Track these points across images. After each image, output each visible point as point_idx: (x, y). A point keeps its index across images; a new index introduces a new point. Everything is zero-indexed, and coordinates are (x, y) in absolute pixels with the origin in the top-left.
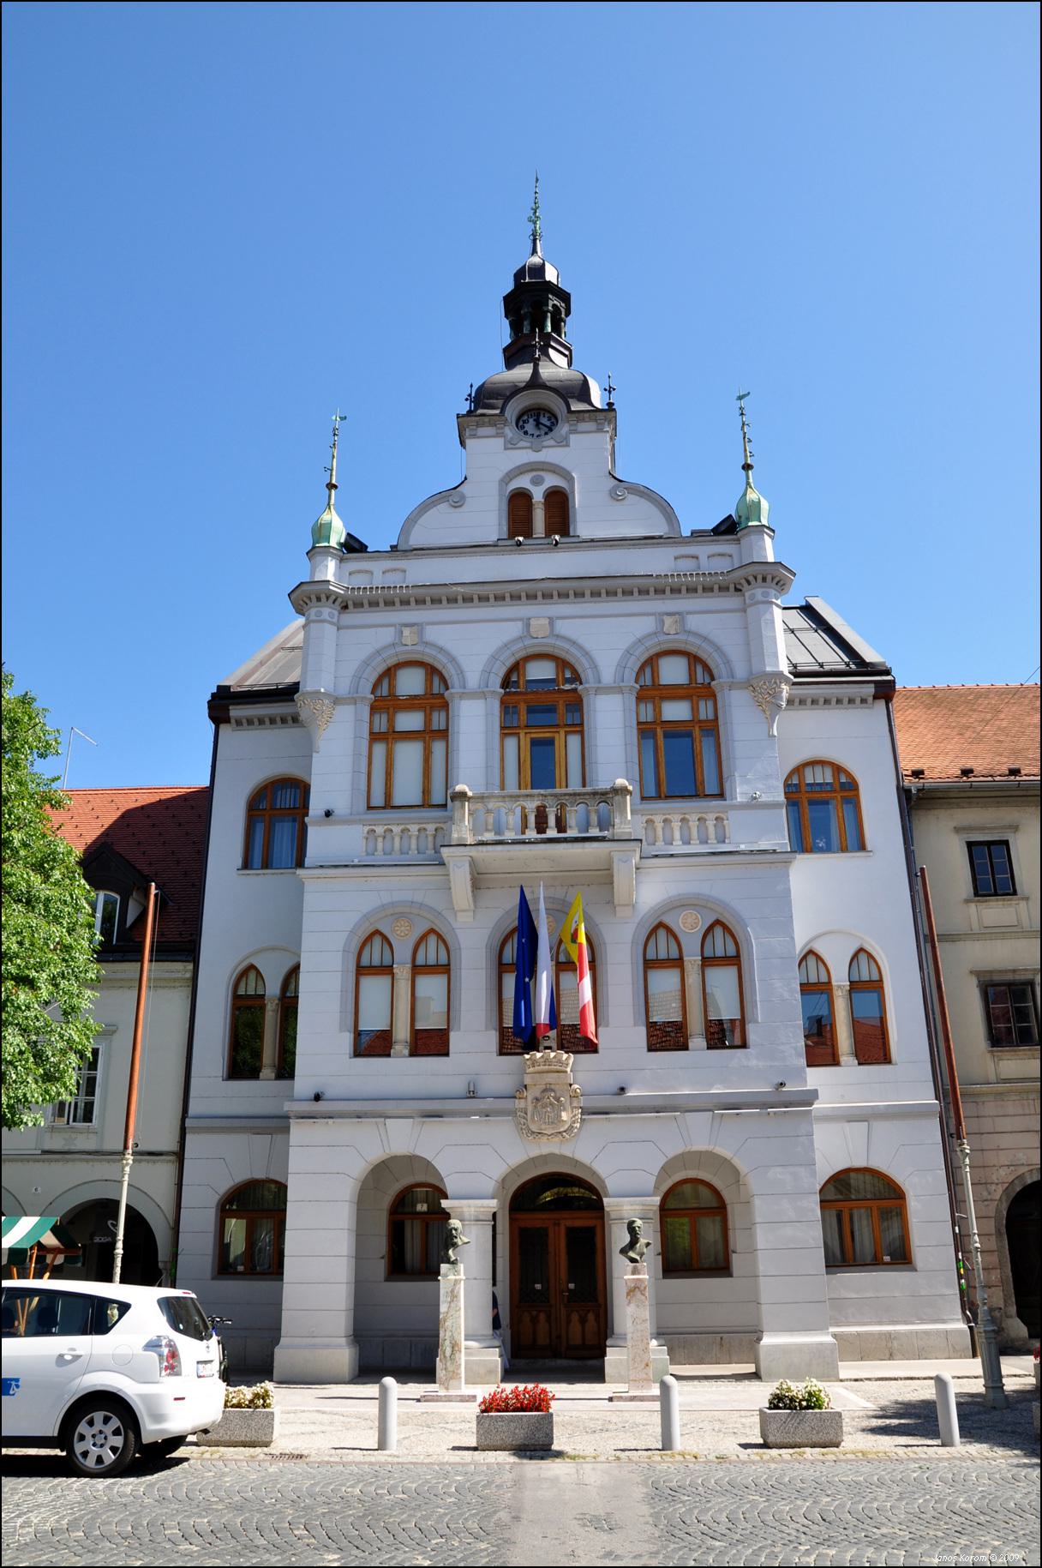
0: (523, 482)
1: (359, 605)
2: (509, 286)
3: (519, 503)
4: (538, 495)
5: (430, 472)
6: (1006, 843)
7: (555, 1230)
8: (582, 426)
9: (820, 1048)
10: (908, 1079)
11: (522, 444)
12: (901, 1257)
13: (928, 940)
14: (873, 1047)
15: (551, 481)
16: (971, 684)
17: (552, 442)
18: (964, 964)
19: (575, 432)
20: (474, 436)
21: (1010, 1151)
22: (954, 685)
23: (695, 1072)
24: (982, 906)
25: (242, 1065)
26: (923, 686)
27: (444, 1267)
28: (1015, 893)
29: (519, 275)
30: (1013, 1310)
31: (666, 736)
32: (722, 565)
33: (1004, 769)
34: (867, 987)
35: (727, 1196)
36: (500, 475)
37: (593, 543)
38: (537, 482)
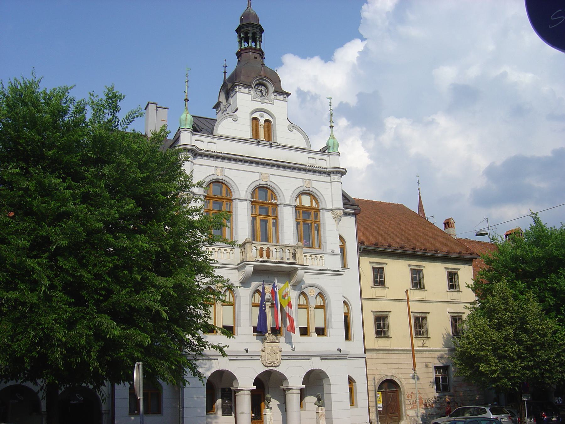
0: (257, 115)
1: (201, 155)
2: (239, 24)
6: (383, 268)
11: (257, 99)
15: (267, 117)
17: (267, 101)
19: (275, 99)
20: (240, 92)
29: (241, 20)
38: (262, 117)
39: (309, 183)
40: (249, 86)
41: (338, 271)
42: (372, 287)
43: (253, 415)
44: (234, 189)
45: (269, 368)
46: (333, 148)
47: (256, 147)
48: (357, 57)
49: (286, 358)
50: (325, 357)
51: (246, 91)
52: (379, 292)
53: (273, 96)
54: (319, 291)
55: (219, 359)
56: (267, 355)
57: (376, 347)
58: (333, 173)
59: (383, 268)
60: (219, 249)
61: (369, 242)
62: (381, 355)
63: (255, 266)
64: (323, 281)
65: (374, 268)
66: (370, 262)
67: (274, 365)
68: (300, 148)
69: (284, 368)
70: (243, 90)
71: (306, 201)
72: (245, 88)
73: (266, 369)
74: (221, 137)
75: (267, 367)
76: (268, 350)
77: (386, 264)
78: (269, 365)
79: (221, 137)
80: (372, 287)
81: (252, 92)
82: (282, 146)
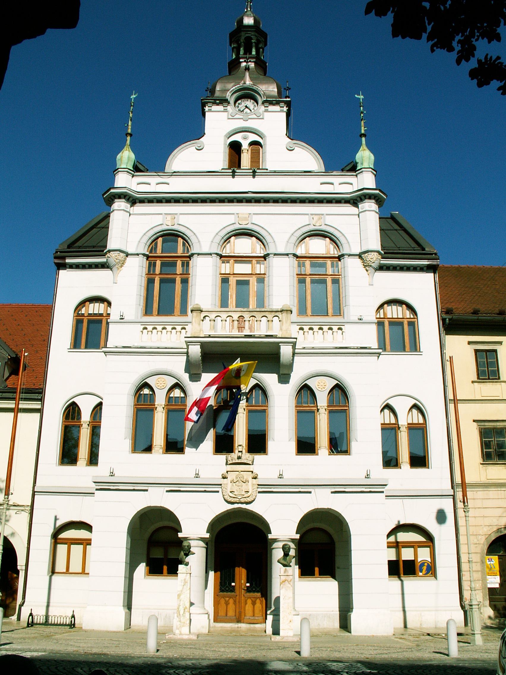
0: (237, 138)
3: (235, 148)
4: (245, 145)
5: (266, 56)
6: (495, 351)
7: (239, 547)
8: (271, 108)
9: (390, 461)
10: (436, 475)
12: (415, 347)
13: (452, 401)
14: (419, 461)
16: (480, 265)
18: (469, 414)
19: (266, 111)
20: (210, 111)
21: (490, 514)
22: (471, 266)
23: (323, 464)
24: (482, 385)
25: (68, 456)
26: (454, 266)
27: (180, 567)
28: (499, 378)
30: (488, 602)
31: (313, 282)
32: (347, 189)
33: (497, 311)
34: (419, 431)
35: (335, 537)
36: (225, 133)
37: (276, 173)
38: (245, 138)
39: (319, 219)
40: (223, 101)
41: (370, 348)
42: (473, 382)
43: (248, 585)
44: (193, 239)
45: (236, 506)
46: (362, 164)
47: (230, 179)
48: (377, 14)
49: (267, 489)
50: (340, 489)
51: (220, 108)
52: (489, 389)
53: (263, 108)
54: (336, 382)
55: (149, 489)
56: (230, 484)
57: (483, 480)
58: (370, 198)
59: (495, 351)
60: (164, 328)
61: (463, 310)
62: (492, 493)
63: (203, 345)
64: (346, 370)
65: (476, 351)
66: (469, 343)
67: (243, 500)
68: (305, 172)
69: (262, 506)
70: (215, 108)
71: (318, 247)
72: (218, 104)
73: (230, 507)
74: (175, 174)
75: (233, 503)
76: (231, 476)
77: (500, 343)
78: (233, 500)
79: (175, 174)
80: (473, 382)
81: (229, 108)
82: (275, 172)
